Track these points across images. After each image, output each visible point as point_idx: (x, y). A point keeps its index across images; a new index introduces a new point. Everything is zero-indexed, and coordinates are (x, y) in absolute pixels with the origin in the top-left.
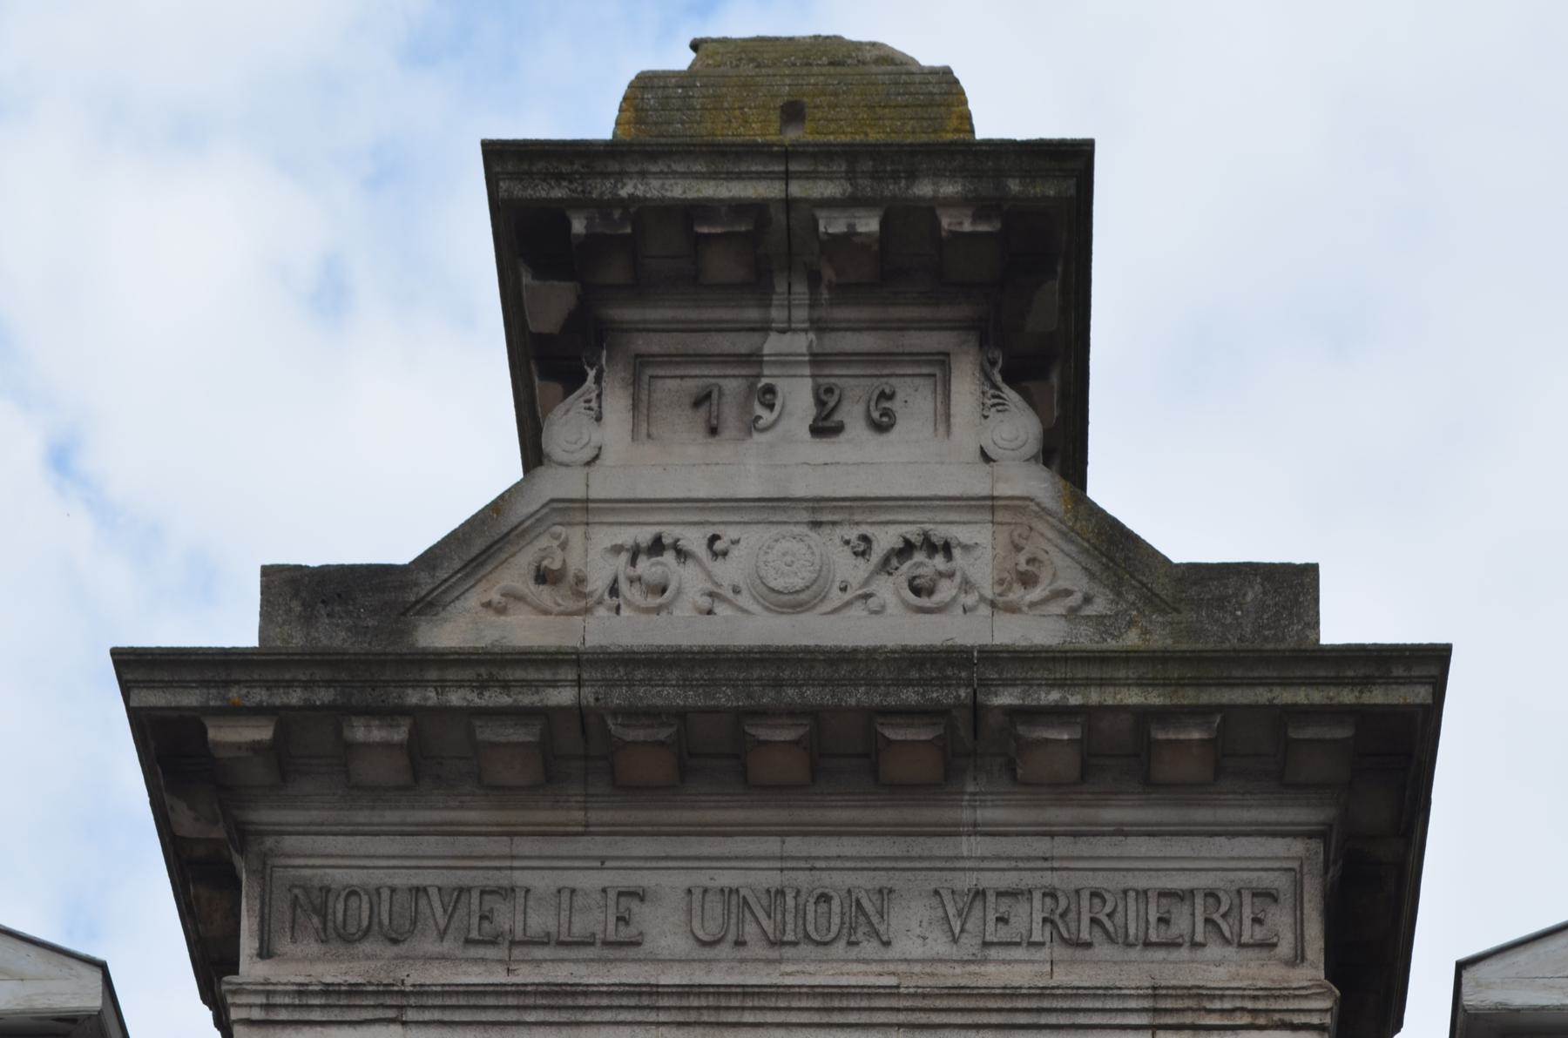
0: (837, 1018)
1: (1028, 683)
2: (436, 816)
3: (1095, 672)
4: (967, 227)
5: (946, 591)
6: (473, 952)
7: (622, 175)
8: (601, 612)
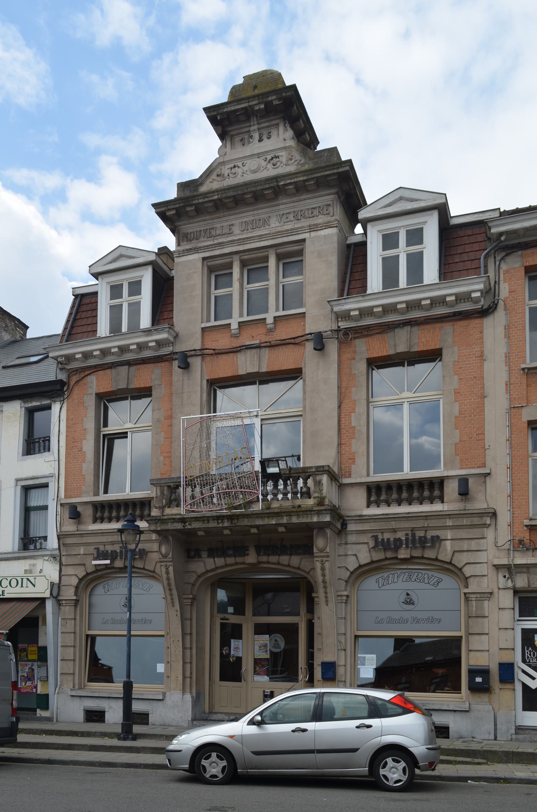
0: (261, 240)
1: (285, 180)
2: (202, 219)
3: (295, 176)
4: (277, 103)
5: (278, 164)
6: (209, 239)
7: (224, 108)
8: (227, 179)
